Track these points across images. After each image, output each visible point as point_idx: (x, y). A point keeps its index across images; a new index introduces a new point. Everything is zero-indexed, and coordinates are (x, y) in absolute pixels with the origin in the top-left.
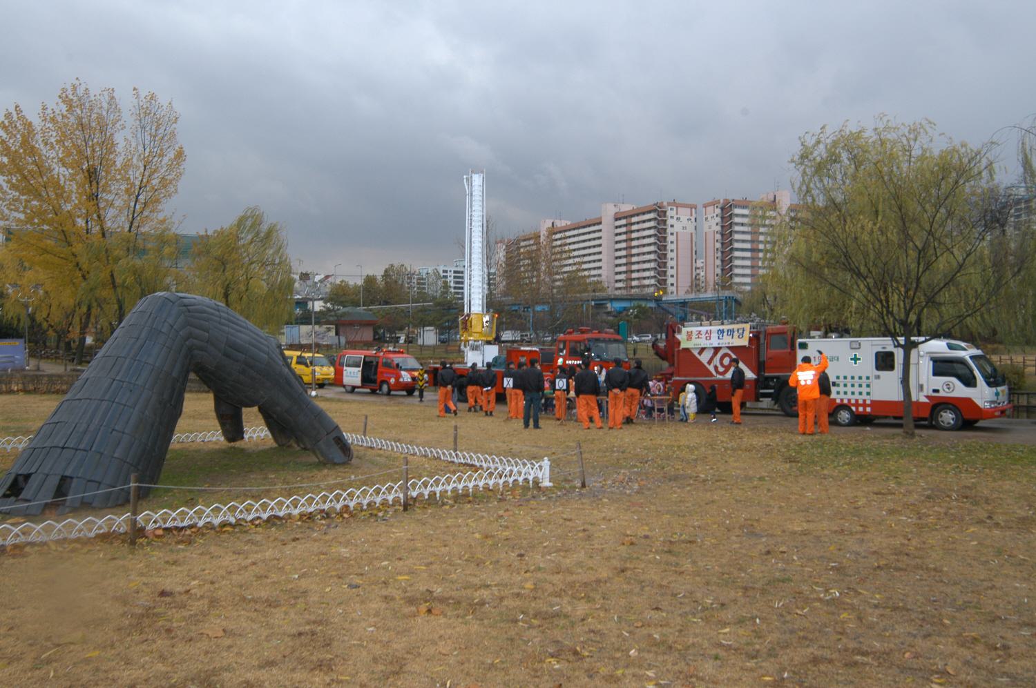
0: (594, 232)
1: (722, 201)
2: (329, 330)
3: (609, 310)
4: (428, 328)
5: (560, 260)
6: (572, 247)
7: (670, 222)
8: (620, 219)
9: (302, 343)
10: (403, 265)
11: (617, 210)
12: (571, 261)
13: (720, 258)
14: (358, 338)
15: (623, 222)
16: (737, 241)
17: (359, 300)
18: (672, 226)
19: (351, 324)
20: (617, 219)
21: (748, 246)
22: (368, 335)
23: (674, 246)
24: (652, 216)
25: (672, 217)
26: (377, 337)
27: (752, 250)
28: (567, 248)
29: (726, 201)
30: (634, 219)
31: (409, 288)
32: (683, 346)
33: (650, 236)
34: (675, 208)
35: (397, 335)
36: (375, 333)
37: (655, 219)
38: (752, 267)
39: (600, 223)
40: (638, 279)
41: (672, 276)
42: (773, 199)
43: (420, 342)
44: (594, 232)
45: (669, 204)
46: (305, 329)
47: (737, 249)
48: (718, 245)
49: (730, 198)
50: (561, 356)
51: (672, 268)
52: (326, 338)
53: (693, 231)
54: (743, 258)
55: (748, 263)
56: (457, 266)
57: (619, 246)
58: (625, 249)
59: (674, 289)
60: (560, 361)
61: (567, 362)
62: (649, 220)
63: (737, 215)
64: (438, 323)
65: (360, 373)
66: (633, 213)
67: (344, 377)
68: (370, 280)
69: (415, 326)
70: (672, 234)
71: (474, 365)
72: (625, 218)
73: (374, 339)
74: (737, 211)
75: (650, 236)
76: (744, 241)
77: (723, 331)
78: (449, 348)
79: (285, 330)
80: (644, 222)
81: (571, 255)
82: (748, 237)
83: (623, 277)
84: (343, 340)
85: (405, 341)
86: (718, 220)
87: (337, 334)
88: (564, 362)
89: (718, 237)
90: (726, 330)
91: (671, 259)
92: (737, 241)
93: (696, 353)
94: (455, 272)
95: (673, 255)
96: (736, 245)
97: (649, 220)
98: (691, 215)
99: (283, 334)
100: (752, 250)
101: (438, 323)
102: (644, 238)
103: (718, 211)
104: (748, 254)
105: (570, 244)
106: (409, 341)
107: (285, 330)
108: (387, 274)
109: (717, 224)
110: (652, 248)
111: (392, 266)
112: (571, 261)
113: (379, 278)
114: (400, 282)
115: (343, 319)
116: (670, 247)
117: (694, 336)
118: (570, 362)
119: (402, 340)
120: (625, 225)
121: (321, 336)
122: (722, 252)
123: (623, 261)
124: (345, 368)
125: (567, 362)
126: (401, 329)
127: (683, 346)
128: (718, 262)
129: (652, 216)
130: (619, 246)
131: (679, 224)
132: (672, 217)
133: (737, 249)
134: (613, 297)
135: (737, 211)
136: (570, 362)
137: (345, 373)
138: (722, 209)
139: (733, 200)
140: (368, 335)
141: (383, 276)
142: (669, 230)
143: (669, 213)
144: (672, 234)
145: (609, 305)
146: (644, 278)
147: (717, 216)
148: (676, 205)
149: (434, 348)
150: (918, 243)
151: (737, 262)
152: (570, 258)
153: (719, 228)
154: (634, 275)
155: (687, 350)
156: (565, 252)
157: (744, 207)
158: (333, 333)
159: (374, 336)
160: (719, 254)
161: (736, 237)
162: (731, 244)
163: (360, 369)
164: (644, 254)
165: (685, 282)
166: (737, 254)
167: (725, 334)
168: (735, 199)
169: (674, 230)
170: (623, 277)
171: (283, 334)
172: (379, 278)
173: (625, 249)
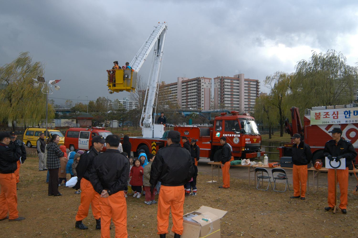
0: (174, 88)
1: (221, 77)
2: (73, 121)
3: (183, 115)
4: (114, 121)
5: (167, 94)
6: (172, 89)
7: (202, 84)
8: (184, 83)
9: (62, 126)
10: (104, 97)
11: (183, 80)
12: (171, 95)
13: (220, 97)
14: (85, 124)
15: (185, 84)
16: (226, 91)
17: (87, 110)
18: (203, 86)
19: (82, 119)
20: (182, 83)
21: (230, 93)
22: (89, 123)
23: (203, 93)
24: (196, 82)
25: (203, 82)
26: (93, 124)
27: (231, 95)
28: (169, 90)
29: (222, 77)
30: (189, 83)
31: (106, 106)
32: (312, 123)
33: (195, 89)
34: (204, 79)
35: (102, 124)
36: (93, 122)
37: (197, 83)
38: (231, 101)
39: (177, 84)
40: (190, 105)
41: (203, 104)
42: (238, 77)
43: (111, 126)
44: (174, 88)
45: (202, 78)
46: (63, 121)
47: (226, 94)
48: (219, 93)
49: (223, 76)
50: (219, 131)
51: (203, 101)
52: (72, 125)
53: (210, 88)
54: (228, 98)
55: (229, 99)
56: (124, 100)
57: (183, 93)
58: (185, 94)
59: (203, 108)
60: (218, 134)
61: (224, 135)
62: (195, 83)
63: (226, 82)
64: (119, 118)
65: (88, 142)
66: (189, 81)
67: (79, 144)
68: (91, 103)
69: (109, 120)
70: (203, 89)
71: (298, 138)
72: (186, 82)
73: (92, 125)
74: (226, 81)
75: (195, 89)
76: (228, 91)
77: (349, 113)
78: (124, 129)
79: (54, 121)
80: (192, 84)
81: (171, 92)
82: (230, 90)
83: (185, 104)
84: (79, 125)
85: (105, 126)
86: (219, 83)
87: (77, 123)
88: (221, 135)
89: (219, 90)
90: (352, 112)
91: (203, 97)
92: (226, 91)
93: (323, 129)
94: (123, 102)
95: (203, 96)
96: (226, 93)
97: (195, 83)
98: (210, 82)
99: (54, 122)
100: (231, 95)
101: (119, 118)
102: (192, 90)
103: (219, 80)
104: (230, 96)
105: (171, 88)
106: (106, 126)
107: (54, 121)
108: (98, 100)
109: (219, 85)
110: (196, 94)
111: (100, 98)
112: (171, 95)
113: (95, 102)
114: (103, 104)
115: (79, 116)
116: (202, 93)
117: (322, 117)
118: (226, 135)
119: (104, 126)
120: (186, 85)
121: (70, 124)
122: (221, 95)
123: (185, 98)
124: (79, 139)
125: (224, 135)
126: (103, 121)
127: (312, 123)
128: (219, 99)
129: (196, 82)
130: (183, 93)
131: (204, 85)
132: (203, 82)
133: (226, 94)
134: (180, 110)
135: (226, 81)
136: (226, 135)
137: (79, 141)
138: (221, 80)
139: (224, 77)
140: (89, 123)
141: (96, 102)
142: (202, 87)
143: (202, 81)
144: (203, 89)
145: (183, 113)
146: (193, 104)
147: (219, 82)
148: (204, 78)
149: (117, 128)
150: (288, 93)
151: (226, 99)
152: (171, 93)
153: (219, 87)
154: (189, 103)
155: (315, 126)
156: (169, 91)
157: (228, 79)
158: (75, 122)
159: (92, 124)
160: (220, 96)
161: (226, 90)
162: (224, 92)
163: (88, 140)
164: (192, 96)
165: (207, 105)
166: (226, 96)
167: (352, 114)
168: (225, 76)
169: (204, 87)
170: (185, 104)
171: (54, 122)
172: (95, 102)
173: (185, 94)
